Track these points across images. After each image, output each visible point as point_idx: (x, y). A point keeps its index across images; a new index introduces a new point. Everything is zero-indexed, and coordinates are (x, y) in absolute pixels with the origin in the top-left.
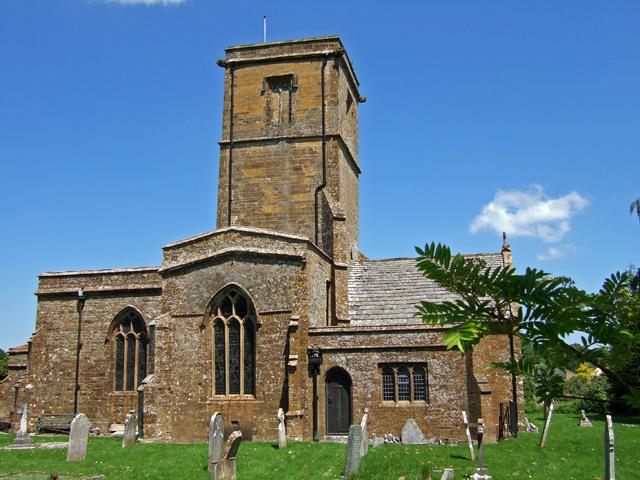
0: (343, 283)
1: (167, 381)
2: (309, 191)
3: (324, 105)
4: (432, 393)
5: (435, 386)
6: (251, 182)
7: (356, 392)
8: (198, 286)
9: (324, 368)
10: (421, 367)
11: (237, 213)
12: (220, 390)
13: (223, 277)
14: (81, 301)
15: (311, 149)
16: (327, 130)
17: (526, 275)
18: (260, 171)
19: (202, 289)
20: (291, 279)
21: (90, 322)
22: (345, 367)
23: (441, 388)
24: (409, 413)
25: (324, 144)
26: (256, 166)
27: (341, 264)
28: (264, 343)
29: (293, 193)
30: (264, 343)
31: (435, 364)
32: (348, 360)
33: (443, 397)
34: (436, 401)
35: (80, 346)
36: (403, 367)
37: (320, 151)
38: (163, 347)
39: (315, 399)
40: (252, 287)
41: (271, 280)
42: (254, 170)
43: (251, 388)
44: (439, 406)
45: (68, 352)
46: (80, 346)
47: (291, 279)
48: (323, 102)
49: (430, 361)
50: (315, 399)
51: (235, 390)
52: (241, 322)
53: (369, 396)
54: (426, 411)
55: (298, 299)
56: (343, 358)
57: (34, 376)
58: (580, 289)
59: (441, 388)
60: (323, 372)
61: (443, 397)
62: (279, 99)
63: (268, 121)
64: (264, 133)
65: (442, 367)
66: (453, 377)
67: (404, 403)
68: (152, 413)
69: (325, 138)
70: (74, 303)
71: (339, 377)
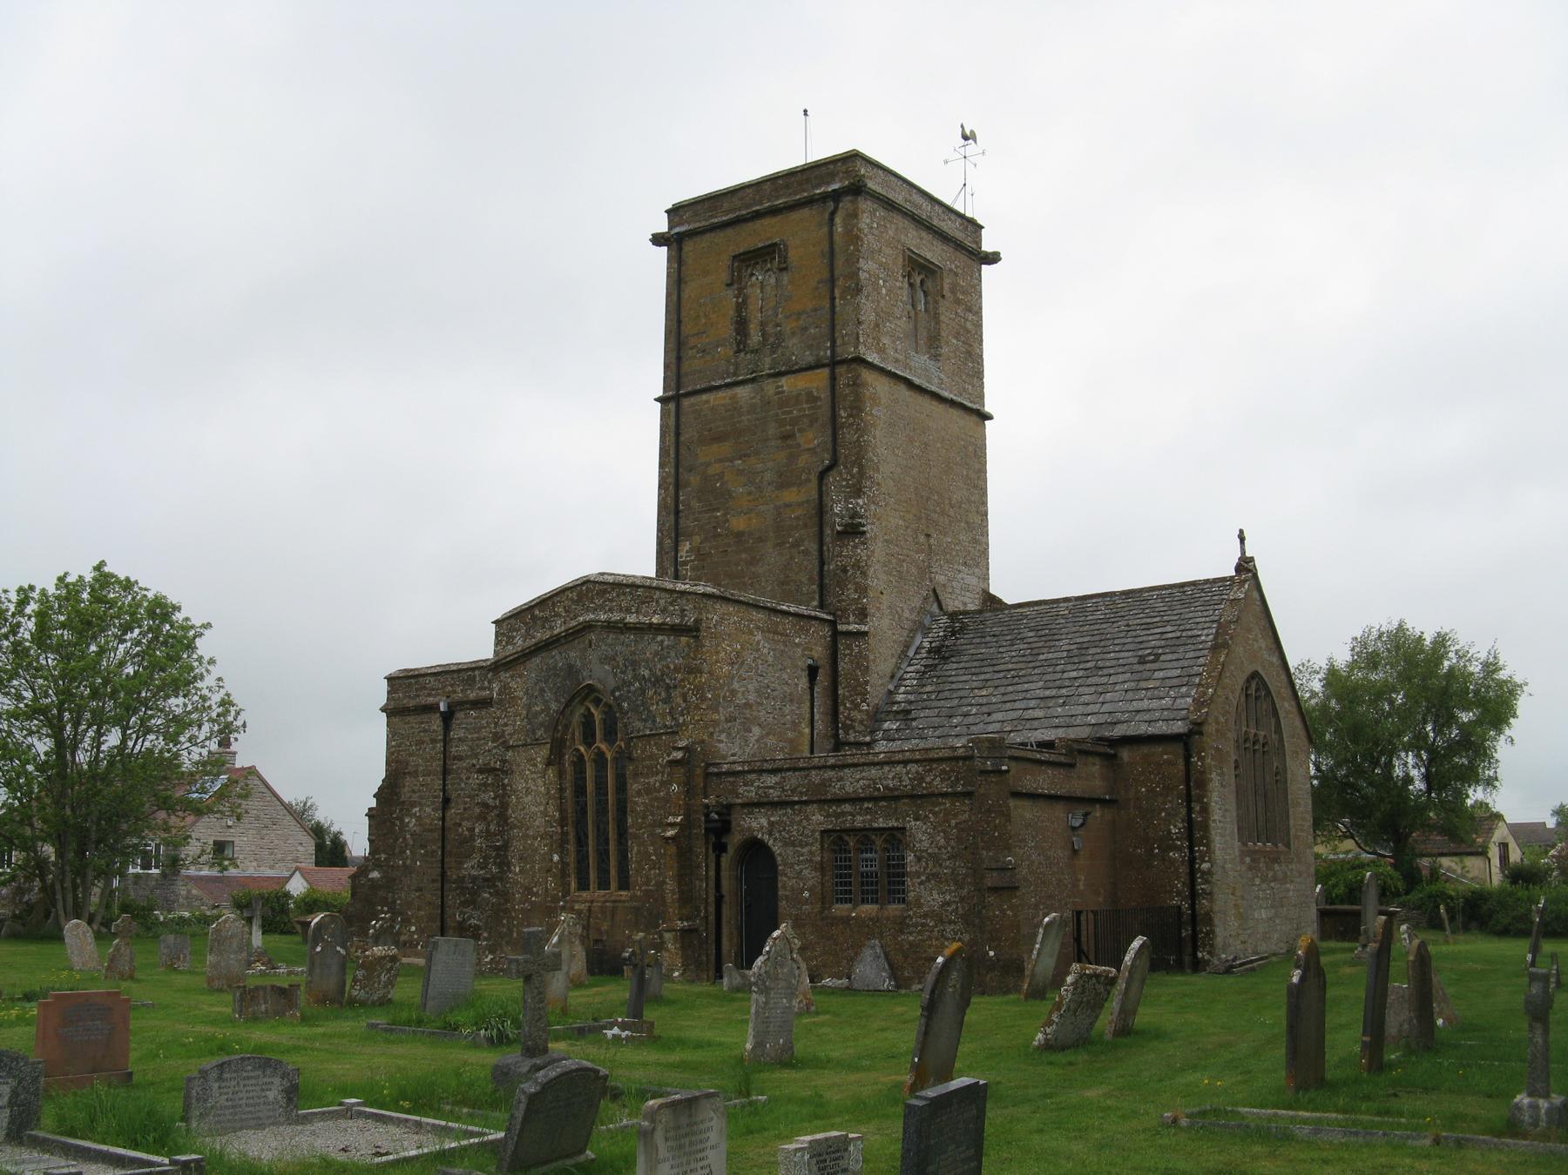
0: (859, 666)
1: (500, 865)
2: (808, 480)
3: (833, 299)
4: (913, 888)
5: (918, 875)
6: (711, 471)
7: (784, 887)
8: (542, 690)
9: (734, 840)
10: (895, 838)
11: (690, 536)
12: (583, 885)
13: (578, 671)
14: (447, 718)
15: (809, 394)
16: (839, 350)
17: (497, 666)
18: (726, 448)
19: (548, 695)
20: (677, 670)
21: (460, 758)
22: (766, 837)
23: (928, 880)
24: (869, 929)
25: (833, 378)
26: (718, 439)
27: (853, 628)
28: (639, 793)
29: (782, 486)
30: (639, 793)
31: (921, 833)
32: (771, 824)
33: (933, 898)
34: (920, 906)
35: (446, 801)
36: (865, 836)
37: (825, 395)
38: (491, 802)
39: (719, 900)
40: (618, 688)
41: (646, 673)
42: (715, 447)
43: (624, 884)
44: (925, 916)
45: (430, 812)
46: (446, 801)
47: (677, 670)
48: (832, 292)
49: (912, 824)
50: (719, 900)
51: (604, 884)
52: (609, 756)
53: (806, 894)
54: (902, 924)
55: (687, 708)
56: (764, 822)
57: (383, 856)
58: (1343, 657)
59: (928, 880)
60: (731, 850)
61: (933, 898)
62: (761, 281)
63: (741, 345)
64: (732, 369)
65: (931, 836)
66: (952, 857)
67: (869, 909)
68: (473, 921)
69: (834, 363)
70: (436, 724)
71: (755, 851)
